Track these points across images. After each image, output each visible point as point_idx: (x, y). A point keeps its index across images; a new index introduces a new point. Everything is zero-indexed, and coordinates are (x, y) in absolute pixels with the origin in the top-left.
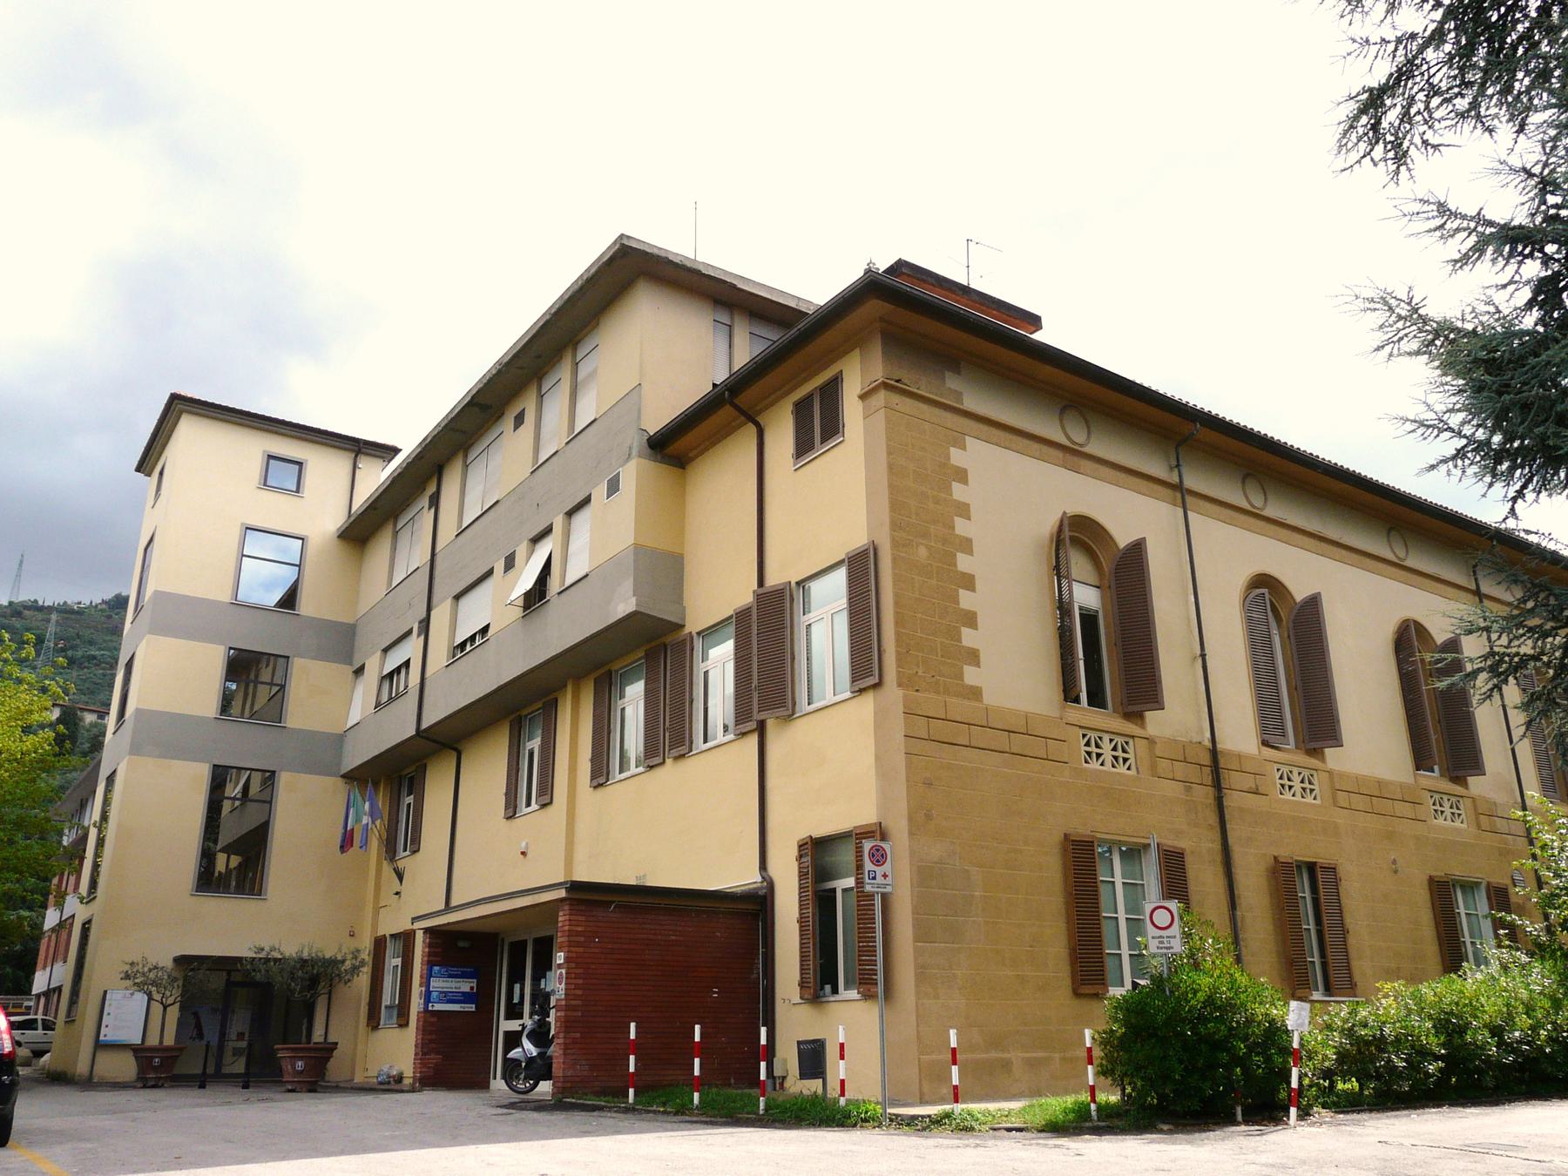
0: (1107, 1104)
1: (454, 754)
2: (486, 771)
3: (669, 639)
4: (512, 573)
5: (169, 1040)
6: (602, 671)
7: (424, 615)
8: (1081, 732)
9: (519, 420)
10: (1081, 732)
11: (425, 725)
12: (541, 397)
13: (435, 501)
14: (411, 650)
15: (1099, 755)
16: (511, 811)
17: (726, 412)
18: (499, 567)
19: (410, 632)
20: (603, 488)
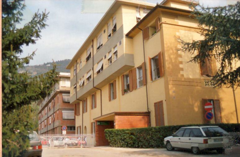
0: (36, 147)
1: (100, 91)
2: (106, 92)
3: (133, 68)
4: (121, 45)
5: (239, 122)
6: (130, 70)
7: (92, 67)
8: (204, 81)
9: (105, 31)
10: (204, 81)
11: (78, 98)
12: (108, 27)
13: (93, 46)
14: (91, 73)
15: (208, 84)
16: (110, 100)
17: (137, 29)
18: (118, 44)
19: (91, 70)
20: (119, 43)
